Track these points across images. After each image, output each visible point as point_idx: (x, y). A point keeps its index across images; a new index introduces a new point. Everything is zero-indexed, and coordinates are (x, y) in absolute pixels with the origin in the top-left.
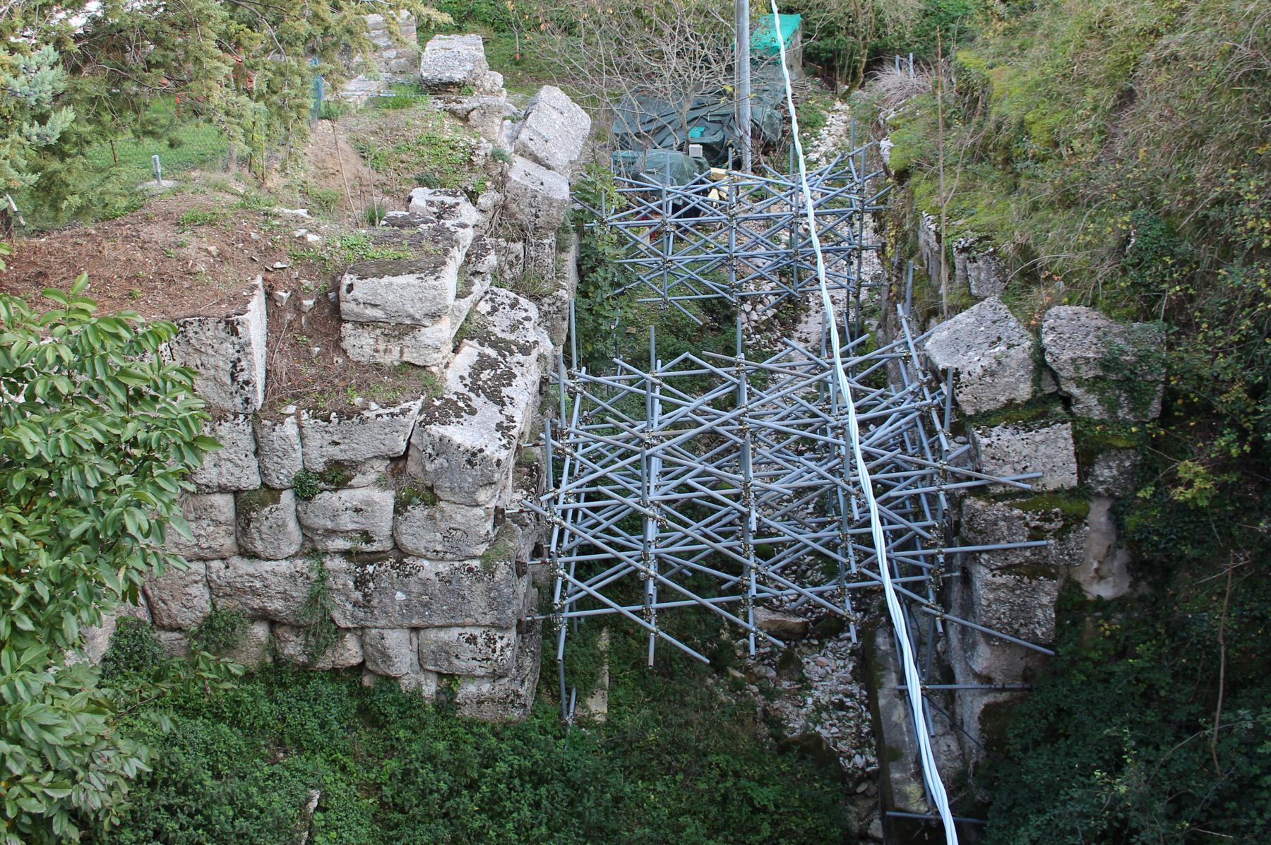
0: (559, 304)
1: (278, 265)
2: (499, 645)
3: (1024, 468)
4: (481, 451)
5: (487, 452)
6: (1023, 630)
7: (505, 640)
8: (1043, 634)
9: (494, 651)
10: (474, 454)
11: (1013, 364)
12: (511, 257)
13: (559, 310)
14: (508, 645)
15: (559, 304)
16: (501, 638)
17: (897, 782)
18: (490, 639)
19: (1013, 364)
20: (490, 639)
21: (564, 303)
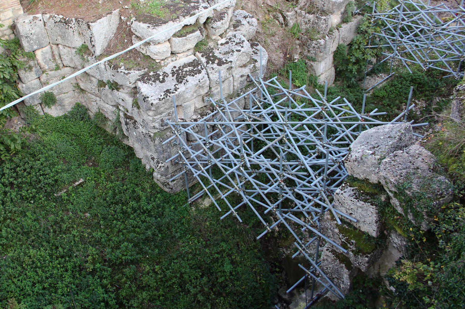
0: (319, 45)
1: (126, 7)
2: (160, 165)
3: (351, 214)
4: (148, 97)
5: (149, 99)
6: (335, 280)
7: (163, 165)
8: (343, 288)
9: (158, 166)
10: (145, 98)
11: (369, 163)
12: (306, 20)
13: (319, 48)
14: (163, 167)
15: (319, 45)
16: (162, 163)
17: (301, 298)
18: (158, 162)
19: (369, 163)
20: (158, 162)
21: (321, 45)
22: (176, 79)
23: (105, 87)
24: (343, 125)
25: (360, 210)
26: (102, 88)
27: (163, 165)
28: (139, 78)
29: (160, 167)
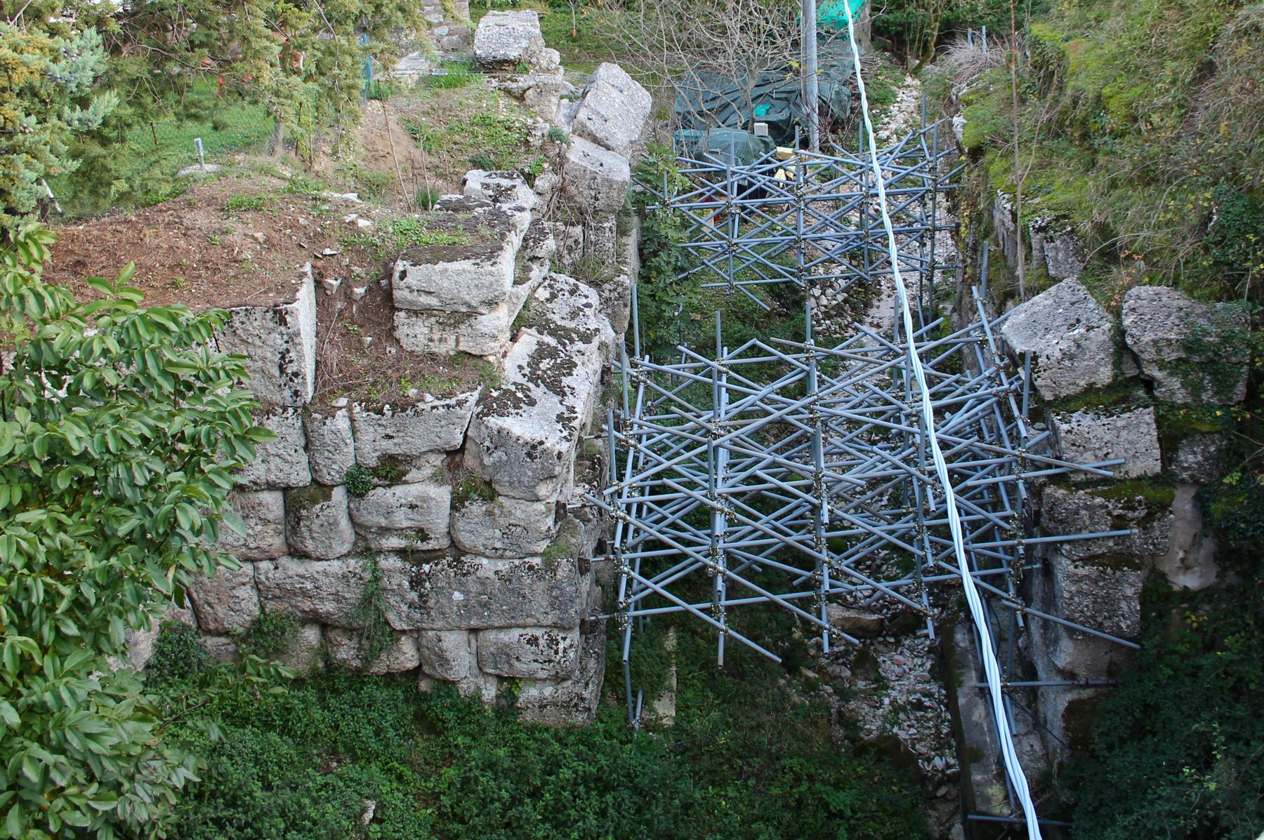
0: (620, 290)
1: (328, 251)
2: (561, 646)
3: (1106, 455)
4: (541, 443)
5: (548, 444)
6: (1107, 624)
7: (568, 641)
8: (1128, 627)
10: (534, 447)
13: (621, 297)
14: (571, 646)
15: (620, 290)
16: (564, 639)
17: (979, 784)
18: (552, 640)
19: (1093, 347)
20: (552, 640)
21: (626, 289)
22: (547, 387)
23: (328, 497)
24: (678, 468)
25: (1124, 433)
26: (318, 507)
27: (568, 641)
28: (479, 409)
29: (565, 650)
